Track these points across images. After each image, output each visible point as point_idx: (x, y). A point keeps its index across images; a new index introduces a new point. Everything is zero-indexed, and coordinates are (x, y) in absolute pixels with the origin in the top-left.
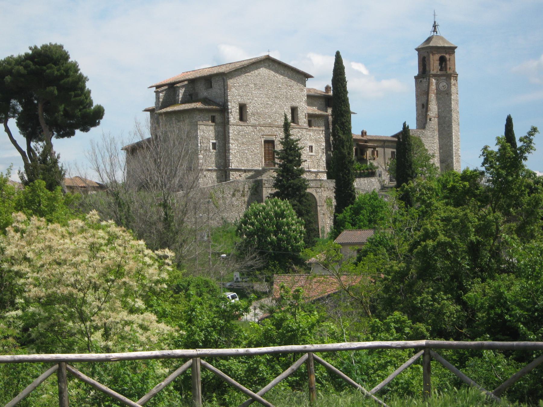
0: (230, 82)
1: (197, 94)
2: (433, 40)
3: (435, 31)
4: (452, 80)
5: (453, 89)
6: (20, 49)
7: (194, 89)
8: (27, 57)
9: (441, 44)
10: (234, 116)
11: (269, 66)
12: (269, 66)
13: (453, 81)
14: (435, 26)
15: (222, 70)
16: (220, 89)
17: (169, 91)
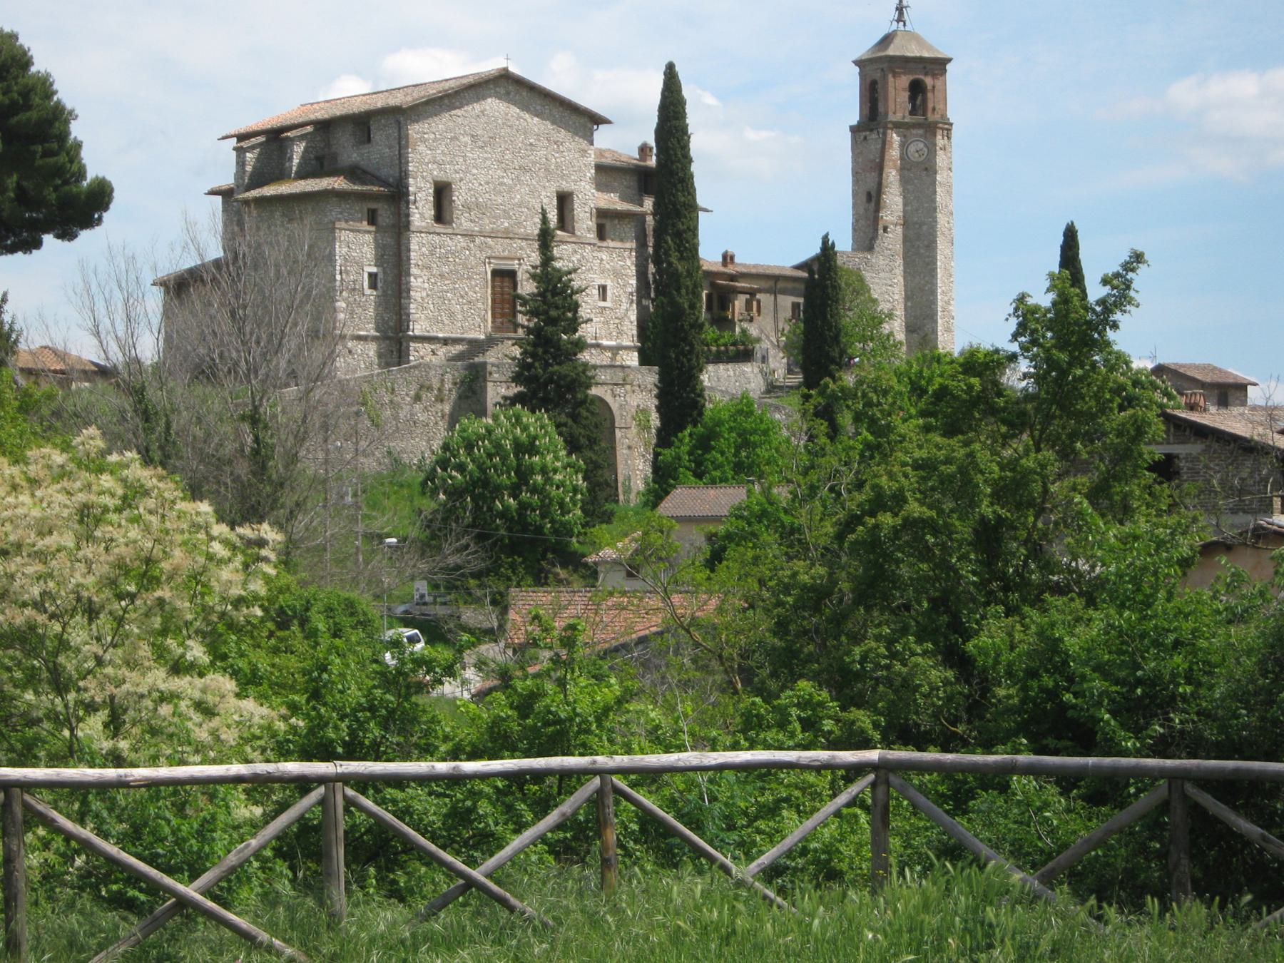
1: (334, 157)
2: (897, 41)
4: (939, 137)
5: (941, 159)
7: (328, 145)
9: (913, 51)
10: (421, 211)
11: (508, 93)
12: (508, 93)
13: (940, 141)
15: (393, 101)
17: (268, 148)
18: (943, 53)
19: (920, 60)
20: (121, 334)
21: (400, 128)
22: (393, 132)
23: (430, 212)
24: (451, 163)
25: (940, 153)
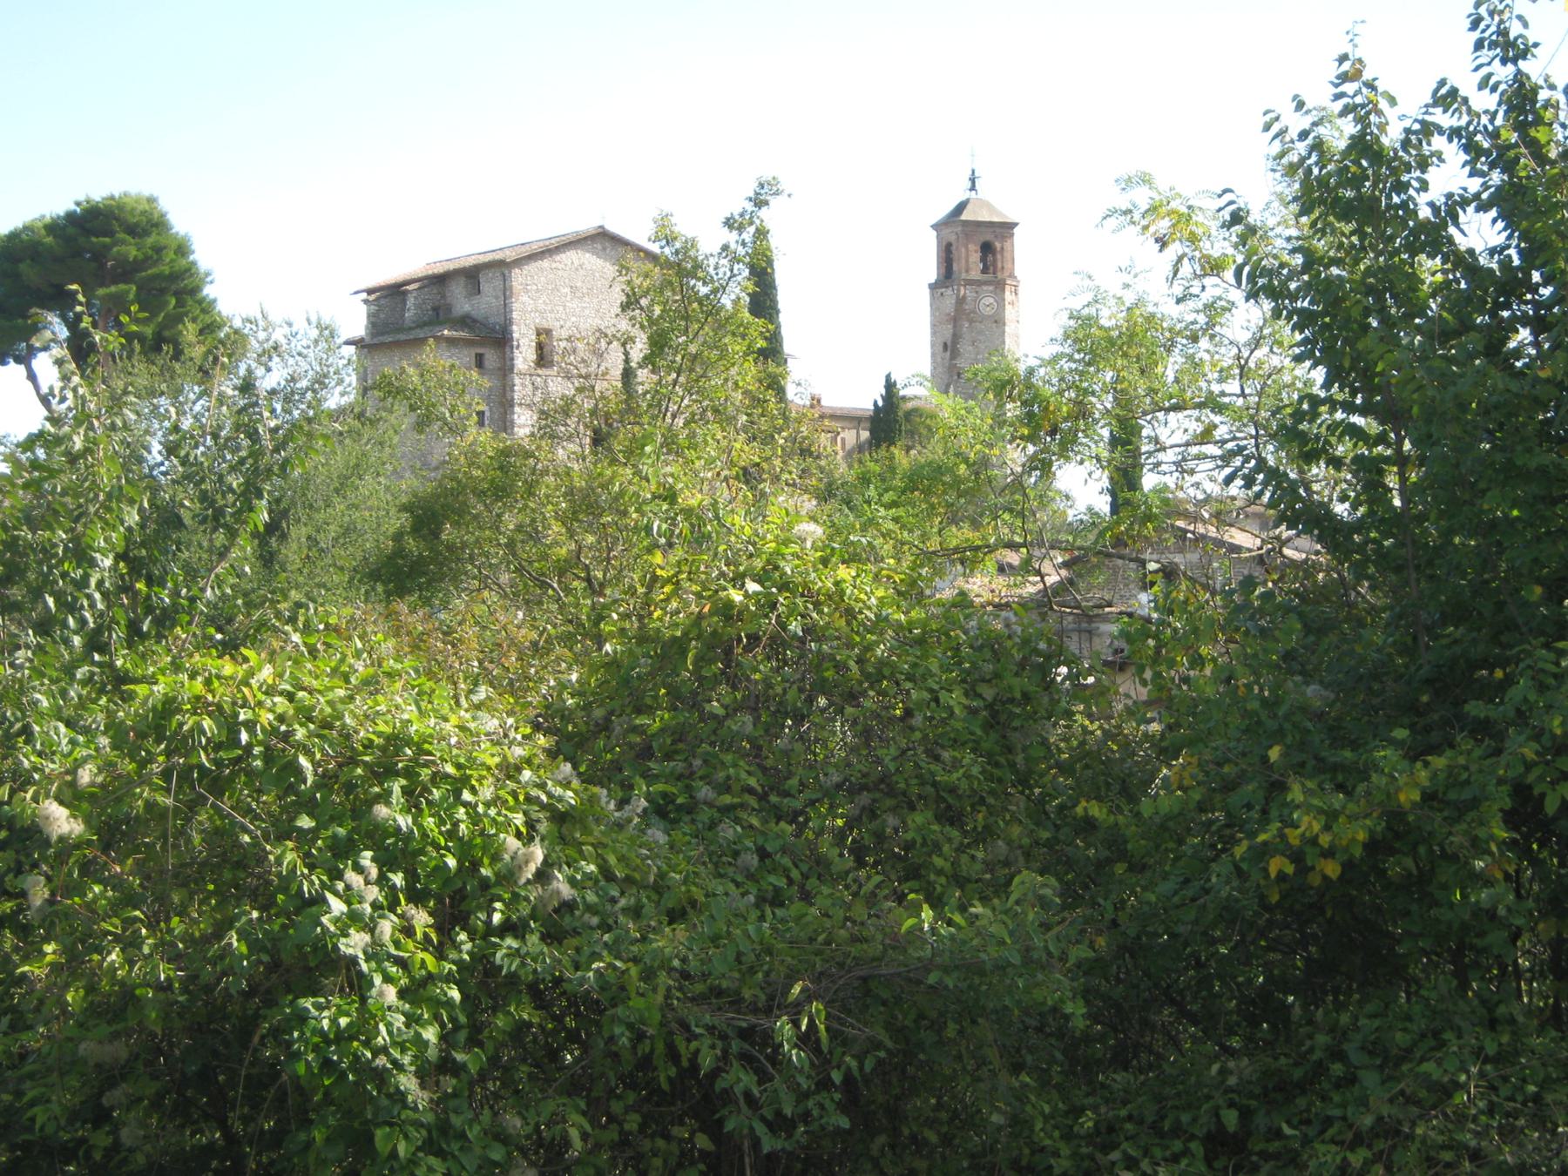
0: (518, 277)
1: (449, 308)
2: (969, 207)
3: (973, 188)
4: (1007, 293)
5: (1009, 313)
6: (57, 202)
7: (444, 297)
8: (70, 216)
9: (984, 216)
10: (524, 357)
11: (604, 249)
12: (604, 249)
13: (1008, 296)
14: (973, 181)
15: (498, 256)
16: (497, 298)
17: (388, 299)
18: (1011, 218)
19: (991, 224)
20: (1211, 465)
21: (505, 279)
22: (498, 283)
23: (532, 356)
24: (552, 311)
25: (1008, 307)
